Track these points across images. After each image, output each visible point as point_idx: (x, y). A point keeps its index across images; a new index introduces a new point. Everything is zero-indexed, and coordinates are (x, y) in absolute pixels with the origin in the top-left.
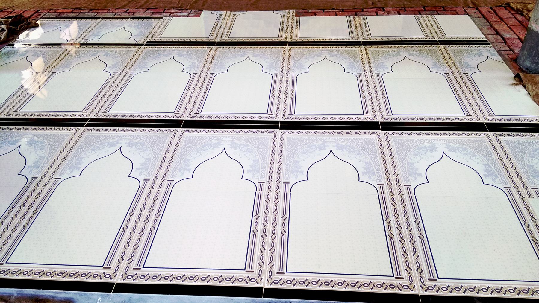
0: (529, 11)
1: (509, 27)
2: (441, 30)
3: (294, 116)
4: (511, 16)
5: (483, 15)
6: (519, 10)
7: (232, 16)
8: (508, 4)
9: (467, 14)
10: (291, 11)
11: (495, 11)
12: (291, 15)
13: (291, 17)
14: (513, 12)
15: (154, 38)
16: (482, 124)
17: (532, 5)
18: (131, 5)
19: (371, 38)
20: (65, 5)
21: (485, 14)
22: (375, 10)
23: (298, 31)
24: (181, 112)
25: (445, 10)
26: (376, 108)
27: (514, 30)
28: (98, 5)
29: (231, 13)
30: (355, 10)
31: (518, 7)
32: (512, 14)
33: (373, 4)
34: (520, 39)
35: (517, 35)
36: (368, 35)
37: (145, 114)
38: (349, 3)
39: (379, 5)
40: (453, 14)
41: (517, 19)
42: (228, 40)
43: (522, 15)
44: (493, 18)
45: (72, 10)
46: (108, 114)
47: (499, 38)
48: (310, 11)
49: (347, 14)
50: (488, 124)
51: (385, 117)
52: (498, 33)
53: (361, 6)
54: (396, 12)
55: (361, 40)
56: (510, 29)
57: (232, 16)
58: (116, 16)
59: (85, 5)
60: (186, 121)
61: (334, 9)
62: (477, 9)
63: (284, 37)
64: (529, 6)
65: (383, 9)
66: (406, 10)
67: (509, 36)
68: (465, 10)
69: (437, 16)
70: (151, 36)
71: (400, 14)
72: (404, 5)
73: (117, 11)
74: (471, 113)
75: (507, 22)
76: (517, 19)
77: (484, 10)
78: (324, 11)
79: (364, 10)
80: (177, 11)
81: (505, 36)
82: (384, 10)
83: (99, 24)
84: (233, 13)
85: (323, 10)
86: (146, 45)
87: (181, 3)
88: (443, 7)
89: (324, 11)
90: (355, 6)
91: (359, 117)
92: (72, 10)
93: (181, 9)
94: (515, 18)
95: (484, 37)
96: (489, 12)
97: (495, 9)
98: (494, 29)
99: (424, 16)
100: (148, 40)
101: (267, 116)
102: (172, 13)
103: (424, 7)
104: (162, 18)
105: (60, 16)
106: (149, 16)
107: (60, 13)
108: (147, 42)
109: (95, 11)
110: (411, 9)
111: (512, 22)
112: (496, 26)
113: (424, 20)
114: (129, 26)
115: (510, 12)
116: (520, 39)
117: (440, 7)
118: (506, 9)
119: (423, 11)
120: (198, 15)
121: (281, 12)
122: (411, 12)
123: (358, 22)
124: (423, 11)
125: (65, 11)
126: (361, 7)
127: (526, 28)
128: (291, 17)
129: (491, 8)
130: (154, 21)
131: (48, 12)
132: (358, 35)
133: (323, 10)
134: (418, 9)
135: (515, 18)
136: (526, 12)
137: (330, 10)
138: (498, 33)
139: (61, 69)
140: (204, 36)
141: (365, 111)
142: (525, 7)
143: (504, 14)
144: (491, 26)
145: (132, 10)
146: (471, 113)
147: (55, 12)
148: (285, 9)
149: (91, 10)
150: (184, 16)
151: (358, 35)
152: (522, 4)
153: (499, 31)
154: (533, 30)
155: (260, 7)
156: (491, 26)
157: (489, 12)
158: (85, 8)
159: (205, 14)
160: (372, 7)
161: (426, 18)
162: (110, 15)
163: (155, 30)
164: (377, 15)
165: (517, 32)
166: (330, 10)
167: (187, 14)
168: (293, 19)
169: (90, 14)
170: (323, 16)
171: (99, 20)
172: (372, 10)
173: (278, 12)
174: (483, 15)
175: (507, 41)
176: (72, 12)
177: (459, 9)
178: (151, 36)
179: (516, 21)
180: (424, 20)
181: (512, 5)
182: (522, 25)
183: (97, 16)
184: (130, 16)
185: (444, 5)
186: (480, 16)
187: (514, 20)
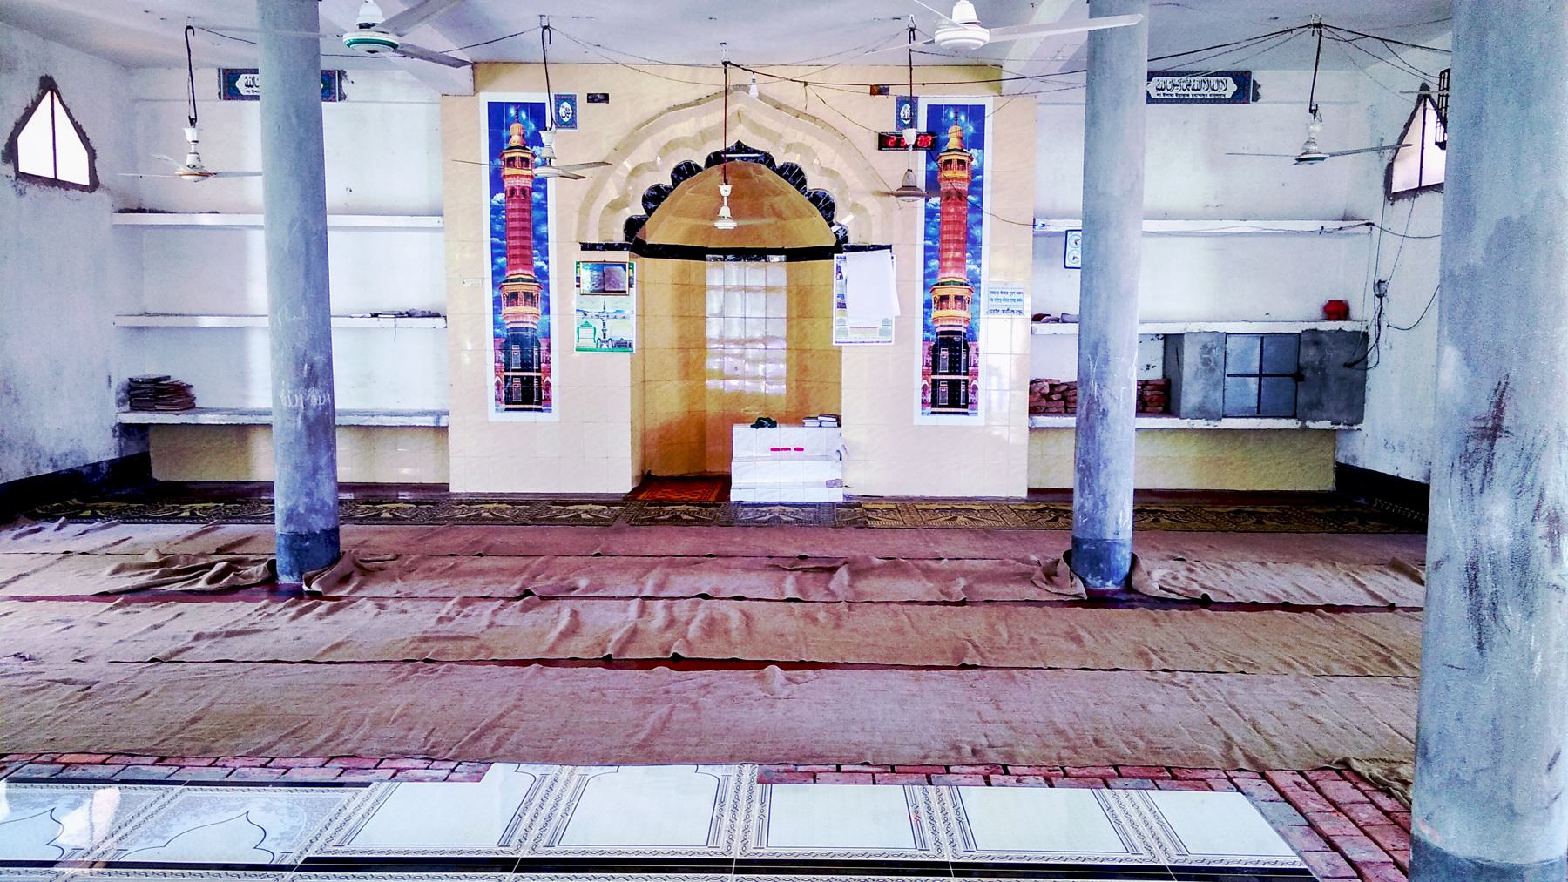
0: (1406, 783)
1: (1361, 829)
2: (1108, 810)
3: (766, 850)
4: (1363, 798)
5: (1282, 794)
6: (1377, 780)
7: (576, 777)
8: (1345, 763)
9: (1239, 790)
10: (747, 768)
11: (1313, 783)
12: (746, 777)
13: (745, 786)
14: (1363, 786)
15: (330, 848)
16: (1163, 868)
17: (1409, 767)
18: (283, 747)
19: (976, 854)
20: (87, 743)
21: (1287, 790)
22: (981, 769)
23: (765, 820)
24: (514, 842)
25: (1174, 777)
26: (943, 836)
27: (1378, 838)
28: (187, 745)
29: (571, 774)
30: (929, 770)
31: (1375, 772)
32: (1362, 792)
33: (974, 752)
34: (1397, 864)
35: (1387, 852)
36: (967, 843)
37: (433, 849)
38: (908, 750)
39: (992, 756)
40: (1198, 789)
41: (1379, 808)
42: (553, 853)
43: (1390, 795)
44: (1313, 804)
45: (104, 757)
46: (346, 848)
47: (1342, 862)
48: (800, 769)
49: (903, 778)
50: (1173, 868)
51: (962, 853)
52: (1335, 848)
53: (943, 757)
54: (1041, 779)
55: (948, 857)
56: (1366, 834)
57: (576, 777)
58: (232, 778)
59: (149, 745)
60: (524, 860)
61: (867, 764)
62: (1264, 776)
63: (722, 844)
64: (1404, 771)
65: (1005, 767)
66: (1066, 775)
67: (1367, 857)
68: (1230, 779)
69: (1154, 794)
70: (322, 841)
71: (1051, 786)
72: (1060, 759)
73: (238, 763)
74: (1141, 849)
75: (1352, 815)
76: (1379, 808)
77: (1284, 780)
78: (838, 770)
79: (952, 769)
80: (415, 763)
81: (1354, 857)
82: (1007, 773)
83: (176, 802)
84: (581, 770)
85: (838, 767)
86: (302, 868)
87: (433, 739)
88: (1169, 769)
89: (838, 770)
90: (925, 757)
91: (908, 852)
92: (104, 757)
93: (430, 758)
94: (1372, 802)
95: (1298, 860)
96: (1298, 784)
97: (1313, 776)
98: (1321, 834)
99: (1120, 792)
100: (311, 854)
101: (707, 850)
102: (399, 770)
103: (1116, 767)
104: (367, 785)
105: (65, 774)
106: (329, 778)
107: (67, 765)
108: (308, 860)
109: (173, 761)
110: (1080, 772)
111: (1366, 813)
112: (1325, 827)
113: (1121, 805)
114: (264, 809)
115: (1355, 787)
116: (1397, 864)
117: (1161, 768)
118: (1345, 779)
119: (1112, 776)
120: (478, 777)
121: (719, 771)
122: (1082, 781)
123: (935, 805)
124: (1112, 776)
125: (86, 758)
126: (944, 762)
127: (1405, 829)
128: (745, 786)
129: (1300, 773)
130: (345, 794)
131: (31, 762)
132: (938, 843)
133: (838, 767)
134: (1099, 772)
135: (1372, 802)
136: (1398, 785)
137: (858, 768)
138: (1335, 848)
139: (142, 840)
140: (486, 842)
141: (921, 844)
142: (1392, 771)
143: (1342, 791)
144: (1312, 825)
145: (284, 762)
146: (1141, 849)
147: (53, 762)
148: (730, 759)
149: (161, 760)
150: (435, 779)
151: (938, 843)
152: (1383, 765)
153: (1337, 840)
154: (1426, 845)
155: (660, 755)
156: (1312, 825)
157: (1298, 784)
158: (143, 753)
159: (498, 769)
160: (974, 761)
161: (1126, 798)
162: (217, 774)
163: (350, 810)
164: (989, 784)
165: (1387, 846)
166: (858, 768)
167: (443, 773)
168: (751, 790)
169: (156, 769)
170: (837, 782)
171: (178, 788)
172: (973, 769)
173: (709, 769)
174: (1282, 794)
175: (1365, 870)
176: (103, 763)
177: (1213, 774)
178: (322, 841)
179: (1379, 813)
180: (1121, 805)
181: (1355, 765)
182: (1396, 823)
183: (174, 778)
184: (273, 778)
185: (1169, 762)
186: (1276, 795)
187: (1370, 807)
